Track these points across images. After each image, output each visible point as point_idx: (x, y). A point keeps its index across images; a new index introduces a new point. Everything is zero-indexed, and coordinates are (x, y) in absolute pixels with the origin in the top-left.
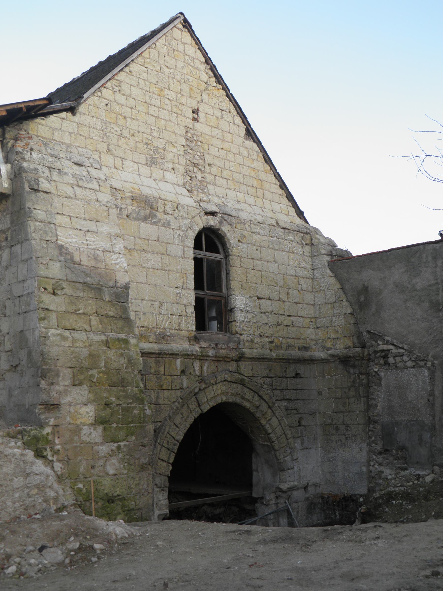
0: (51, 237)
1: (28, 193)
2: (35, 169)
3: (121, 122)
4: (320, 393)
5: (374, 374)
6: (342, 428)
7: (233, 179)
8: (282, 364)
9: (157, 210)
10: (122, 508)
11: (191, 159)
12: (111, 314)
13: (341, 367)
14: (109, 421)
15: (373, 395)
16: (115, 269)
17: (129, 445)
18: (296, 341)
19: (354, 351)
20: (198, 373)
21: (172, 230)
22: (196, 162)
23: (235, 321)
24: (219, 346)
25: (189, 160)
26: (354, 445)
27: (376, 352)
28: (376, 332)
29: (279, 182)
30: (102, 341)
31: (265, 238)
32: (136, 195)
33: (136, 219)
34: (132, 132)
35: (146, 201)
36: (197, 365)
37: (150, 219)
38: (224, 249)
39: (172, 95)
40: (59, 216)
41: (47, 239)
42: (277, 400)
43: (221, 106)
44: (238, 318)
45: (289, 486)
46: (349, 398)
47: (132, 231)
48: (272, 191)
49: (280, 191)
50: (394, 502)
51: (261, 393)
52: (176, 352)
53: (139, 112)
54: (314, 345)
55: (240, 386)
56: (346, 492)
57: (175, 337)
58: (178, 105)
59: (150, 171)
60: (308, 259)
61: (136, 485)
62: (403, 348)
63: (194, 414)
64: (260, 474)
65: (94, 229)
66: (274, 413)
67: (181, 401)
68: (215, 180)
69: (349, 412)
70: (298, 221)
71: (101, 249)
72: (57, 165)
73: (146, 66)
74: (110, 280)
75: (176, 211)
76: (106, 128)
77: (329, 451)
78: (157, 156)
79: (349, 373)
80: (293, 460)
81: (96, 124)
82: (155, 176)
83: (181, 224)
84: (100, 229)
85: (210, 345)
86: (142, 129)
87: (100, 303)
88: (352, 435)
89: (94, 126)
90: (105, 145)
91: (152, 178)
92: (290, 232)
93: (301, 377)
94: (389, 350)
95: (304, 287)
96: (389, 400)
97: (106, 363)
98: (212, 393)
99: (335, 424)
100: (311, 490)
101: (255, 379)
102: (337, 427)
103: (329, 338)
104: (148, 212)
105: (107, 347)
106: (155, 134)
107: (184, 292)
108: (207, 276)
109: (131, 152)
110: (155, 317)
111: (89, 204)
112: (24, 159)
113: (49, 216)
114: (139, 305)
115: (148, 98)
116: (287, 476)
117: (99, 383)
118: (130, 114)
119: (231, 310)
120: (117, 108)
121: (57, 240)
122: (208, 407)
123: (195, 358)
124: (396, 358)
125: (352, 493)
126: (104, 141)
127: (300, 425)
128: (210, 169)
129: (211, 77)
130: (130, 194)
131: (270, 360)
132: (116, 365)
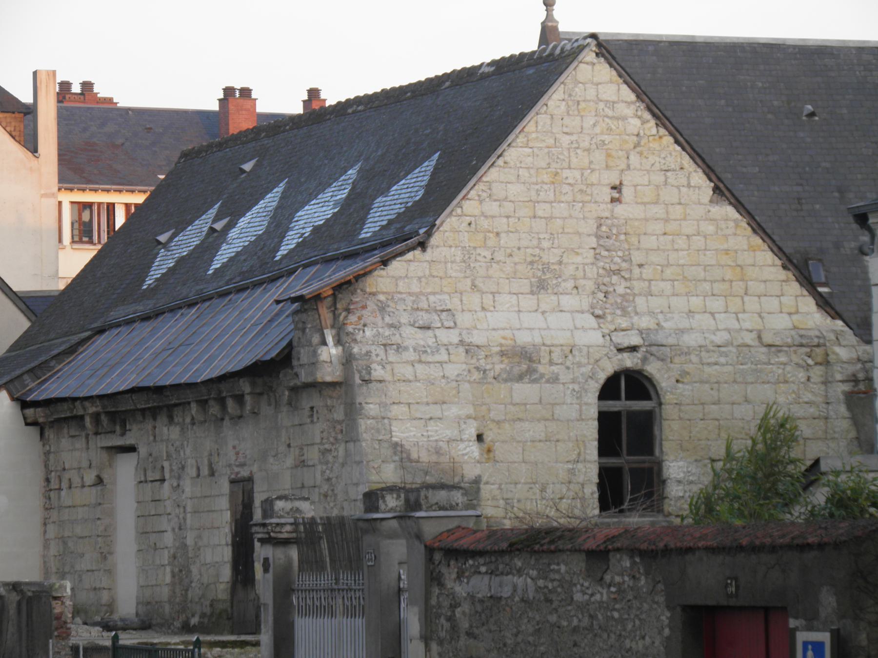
0: (384, 435)
1: (361, 385)
2: (368, 353)
3: (492, 241)
7: (685, 277)
9: (540, 362)
11: (607, 266)
21: (561, 386)
22: (614, 267)
25: (603, 268)
31: (730, 368)
32: (506, 348)
33: (506, 381)
34: (509, 251)
35: (521, 353)
37: (528, 377)
39: (572, 175)
40: (395, 407)
41: (380, 438)
43: (664, 164)
44: (673, 493)
47: (502, 396)
48: (764, 279)
53: (519, 220)
58: (584, 188)
59: (536, 301)
65: (438, 414)
68: (649, 287)
72: (396, 339)
73: (531, 144)
75: (570, 357)
76: (469, 258)
78: (548, 276)
81: (454, 255)
82: (544, 306)
83: (577, 374)
84: (446, 414)
86: (524, 243)
89: (453, 259)
90: (469, 282)
91: (540, 310)
92: (780, 351)
104: (524, 367)
106: (546, 244)
108: (628, 436)
109: (507, 281)
110: (535, 504)
111: (433, 384)
112: (355, 341)
113: (382, 410)
114: (511, 491)
115: (533, 193)
118: (506, 226)
119: (664, 482)
120: (485, 223)
121: (391, 437)
126: (467, 275)
128: (641, 273)
129: (648, 121)
130: (498, 349)
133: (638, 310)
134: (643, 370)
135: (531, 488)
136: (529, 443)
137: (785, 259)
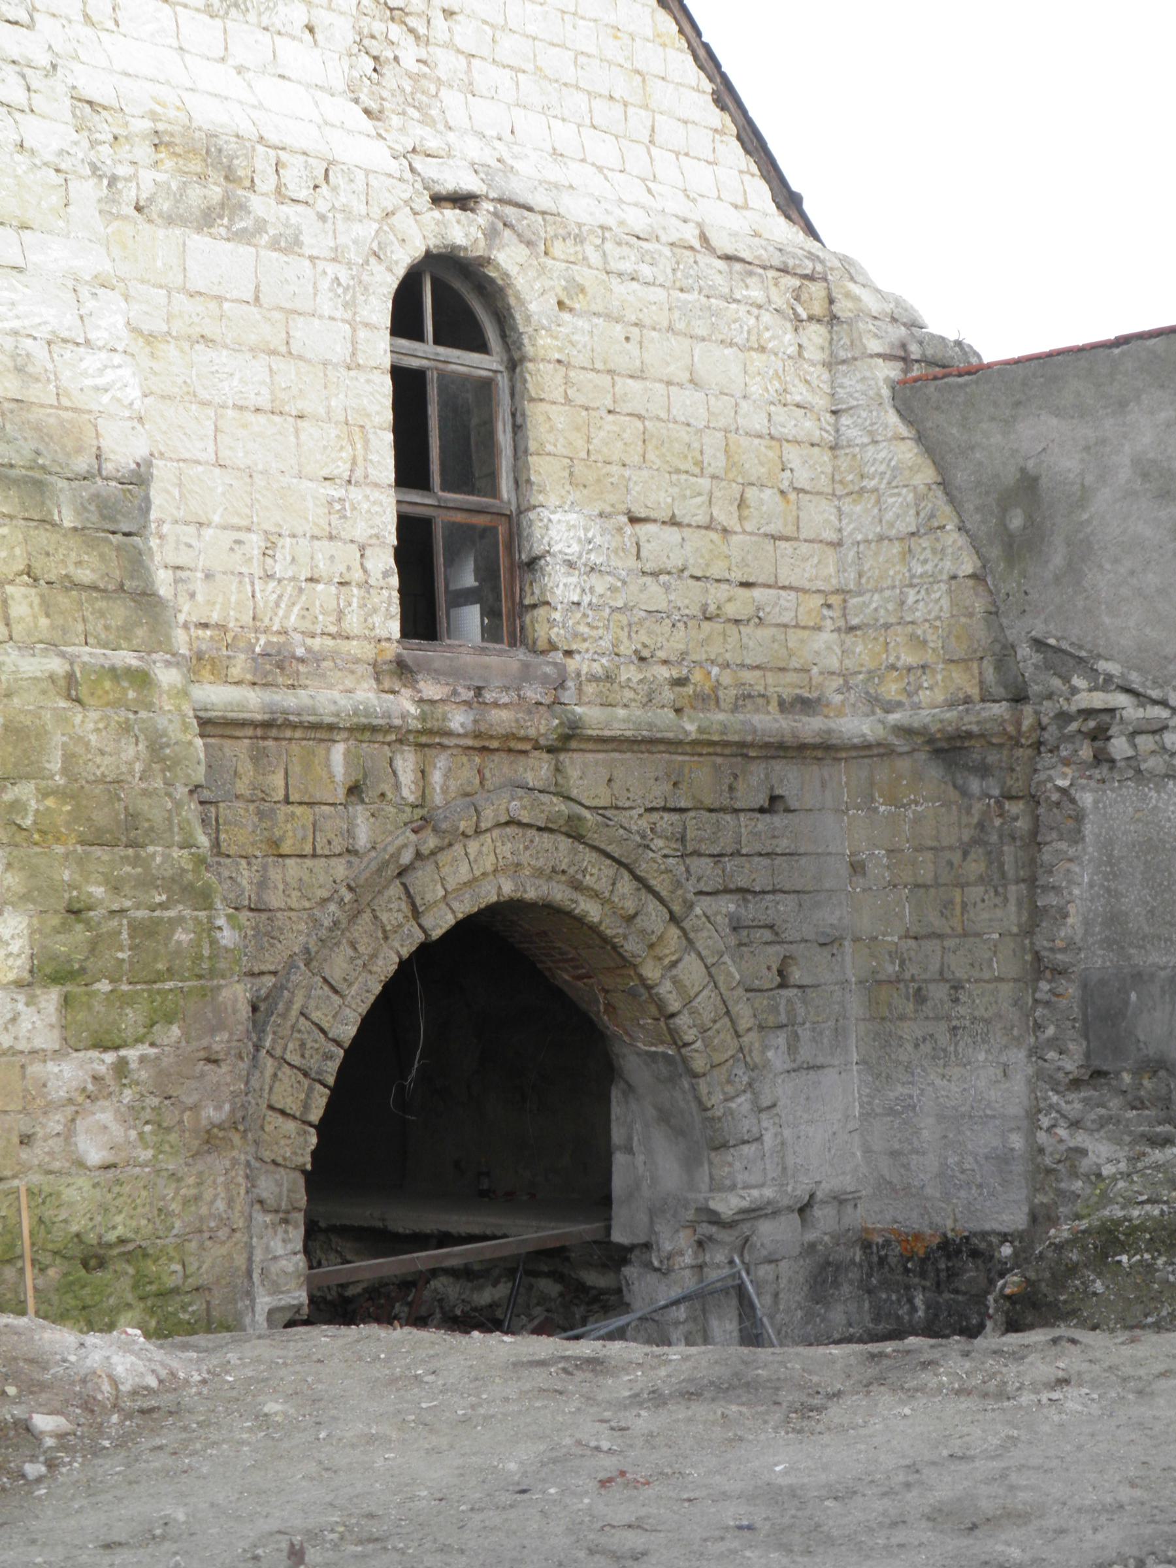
4: (857, 868)
5: (1055, 797)
6: (938, 992)
7: (538, 69)
8: (719, 760)
10: (135, 1287)
12: (85, 575)
13: (935, 772)
14: (83, 970)
15: (1051, 872)
16: (94, 407)
17: (158, 1058)
18: (771, 678)
19: (984, 714)
20: (409, 793)
21: (307, 263)
23: (548, 603)
24: (489, 696)
26: (981, 1057)
27: (1064, 717)
28: (1065, 645)
29: (711, 80)
30: (52, 678)
31: (658, 294)
32: (170, 128)
33: (170, 220)
36: (406, 764)
37: (225, 221)
38: (504, 336)
42: (701, 893)
44: (558, 592)
45: (745, 1204)
46: (962, 886)
47: (159, 264)
49: (717, 118)
50: (1124, 1258)
51: (642, 869)
52: (328, 720)
54: (838, 691)
55: (564, 843)
56: (949, 1224)
57: (325, 664)
60: (820, 375)
61: (186, 1202)
62: (1164, 703)
63: (397, 944)
64: (640, 1158)
66: (690, 941)
67: (348, 897)
69: (965, 935)
70: (783, 230)
71: (43, 333)
74: (79, 450)
75: (324, 189)
77: (888, 1077)
79: (964, 792)
80: (761, 1110)
83: (342, 239)
85: (455, 693)
87: (43, 537)
88: (974, 1020)
91: (231, 62)
92: (751, 274)
93: (788, 810)
94: (1111, 711)
95: (803, 478)
96: (1108, 890)
97: (69, 758)
98: (464, 869)
99: (913, 979)
100: (825, 1217)
101: (622, 817)
102: (919, 989)
103: (893, 667)
104: (216, 192)
105: (69, 697)
107: (355, 494)
114: (190, 546)
116: (738, 1165)
117: (40, 831)
122: (449, 921)
123: (400, 741)
124: (1140, 740)
125: (974, 1226)
127: (783, 985)
130: (147, 125)
131: (673, 745)
132: (105, 766)
133: (451, 124)
134: (489, 261)
135: (238, 542)
136: (230, 413)
137: (718, 80)
